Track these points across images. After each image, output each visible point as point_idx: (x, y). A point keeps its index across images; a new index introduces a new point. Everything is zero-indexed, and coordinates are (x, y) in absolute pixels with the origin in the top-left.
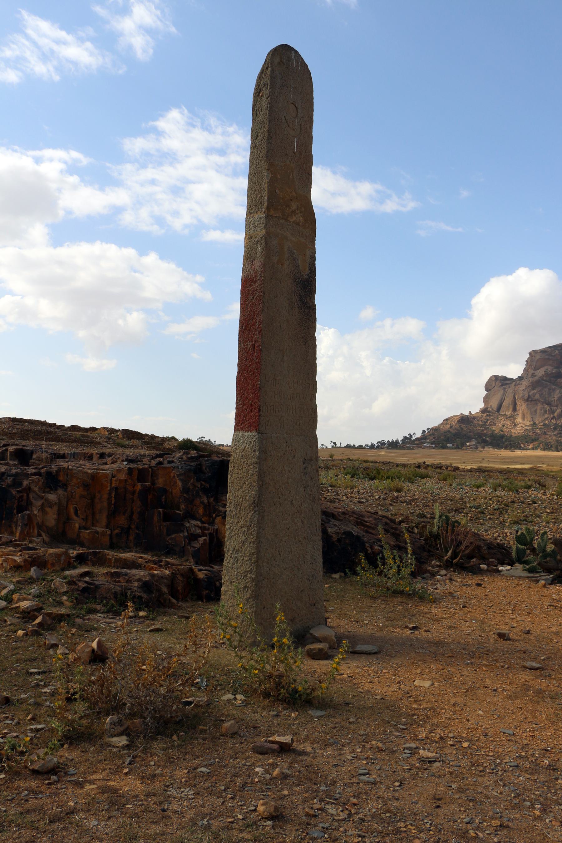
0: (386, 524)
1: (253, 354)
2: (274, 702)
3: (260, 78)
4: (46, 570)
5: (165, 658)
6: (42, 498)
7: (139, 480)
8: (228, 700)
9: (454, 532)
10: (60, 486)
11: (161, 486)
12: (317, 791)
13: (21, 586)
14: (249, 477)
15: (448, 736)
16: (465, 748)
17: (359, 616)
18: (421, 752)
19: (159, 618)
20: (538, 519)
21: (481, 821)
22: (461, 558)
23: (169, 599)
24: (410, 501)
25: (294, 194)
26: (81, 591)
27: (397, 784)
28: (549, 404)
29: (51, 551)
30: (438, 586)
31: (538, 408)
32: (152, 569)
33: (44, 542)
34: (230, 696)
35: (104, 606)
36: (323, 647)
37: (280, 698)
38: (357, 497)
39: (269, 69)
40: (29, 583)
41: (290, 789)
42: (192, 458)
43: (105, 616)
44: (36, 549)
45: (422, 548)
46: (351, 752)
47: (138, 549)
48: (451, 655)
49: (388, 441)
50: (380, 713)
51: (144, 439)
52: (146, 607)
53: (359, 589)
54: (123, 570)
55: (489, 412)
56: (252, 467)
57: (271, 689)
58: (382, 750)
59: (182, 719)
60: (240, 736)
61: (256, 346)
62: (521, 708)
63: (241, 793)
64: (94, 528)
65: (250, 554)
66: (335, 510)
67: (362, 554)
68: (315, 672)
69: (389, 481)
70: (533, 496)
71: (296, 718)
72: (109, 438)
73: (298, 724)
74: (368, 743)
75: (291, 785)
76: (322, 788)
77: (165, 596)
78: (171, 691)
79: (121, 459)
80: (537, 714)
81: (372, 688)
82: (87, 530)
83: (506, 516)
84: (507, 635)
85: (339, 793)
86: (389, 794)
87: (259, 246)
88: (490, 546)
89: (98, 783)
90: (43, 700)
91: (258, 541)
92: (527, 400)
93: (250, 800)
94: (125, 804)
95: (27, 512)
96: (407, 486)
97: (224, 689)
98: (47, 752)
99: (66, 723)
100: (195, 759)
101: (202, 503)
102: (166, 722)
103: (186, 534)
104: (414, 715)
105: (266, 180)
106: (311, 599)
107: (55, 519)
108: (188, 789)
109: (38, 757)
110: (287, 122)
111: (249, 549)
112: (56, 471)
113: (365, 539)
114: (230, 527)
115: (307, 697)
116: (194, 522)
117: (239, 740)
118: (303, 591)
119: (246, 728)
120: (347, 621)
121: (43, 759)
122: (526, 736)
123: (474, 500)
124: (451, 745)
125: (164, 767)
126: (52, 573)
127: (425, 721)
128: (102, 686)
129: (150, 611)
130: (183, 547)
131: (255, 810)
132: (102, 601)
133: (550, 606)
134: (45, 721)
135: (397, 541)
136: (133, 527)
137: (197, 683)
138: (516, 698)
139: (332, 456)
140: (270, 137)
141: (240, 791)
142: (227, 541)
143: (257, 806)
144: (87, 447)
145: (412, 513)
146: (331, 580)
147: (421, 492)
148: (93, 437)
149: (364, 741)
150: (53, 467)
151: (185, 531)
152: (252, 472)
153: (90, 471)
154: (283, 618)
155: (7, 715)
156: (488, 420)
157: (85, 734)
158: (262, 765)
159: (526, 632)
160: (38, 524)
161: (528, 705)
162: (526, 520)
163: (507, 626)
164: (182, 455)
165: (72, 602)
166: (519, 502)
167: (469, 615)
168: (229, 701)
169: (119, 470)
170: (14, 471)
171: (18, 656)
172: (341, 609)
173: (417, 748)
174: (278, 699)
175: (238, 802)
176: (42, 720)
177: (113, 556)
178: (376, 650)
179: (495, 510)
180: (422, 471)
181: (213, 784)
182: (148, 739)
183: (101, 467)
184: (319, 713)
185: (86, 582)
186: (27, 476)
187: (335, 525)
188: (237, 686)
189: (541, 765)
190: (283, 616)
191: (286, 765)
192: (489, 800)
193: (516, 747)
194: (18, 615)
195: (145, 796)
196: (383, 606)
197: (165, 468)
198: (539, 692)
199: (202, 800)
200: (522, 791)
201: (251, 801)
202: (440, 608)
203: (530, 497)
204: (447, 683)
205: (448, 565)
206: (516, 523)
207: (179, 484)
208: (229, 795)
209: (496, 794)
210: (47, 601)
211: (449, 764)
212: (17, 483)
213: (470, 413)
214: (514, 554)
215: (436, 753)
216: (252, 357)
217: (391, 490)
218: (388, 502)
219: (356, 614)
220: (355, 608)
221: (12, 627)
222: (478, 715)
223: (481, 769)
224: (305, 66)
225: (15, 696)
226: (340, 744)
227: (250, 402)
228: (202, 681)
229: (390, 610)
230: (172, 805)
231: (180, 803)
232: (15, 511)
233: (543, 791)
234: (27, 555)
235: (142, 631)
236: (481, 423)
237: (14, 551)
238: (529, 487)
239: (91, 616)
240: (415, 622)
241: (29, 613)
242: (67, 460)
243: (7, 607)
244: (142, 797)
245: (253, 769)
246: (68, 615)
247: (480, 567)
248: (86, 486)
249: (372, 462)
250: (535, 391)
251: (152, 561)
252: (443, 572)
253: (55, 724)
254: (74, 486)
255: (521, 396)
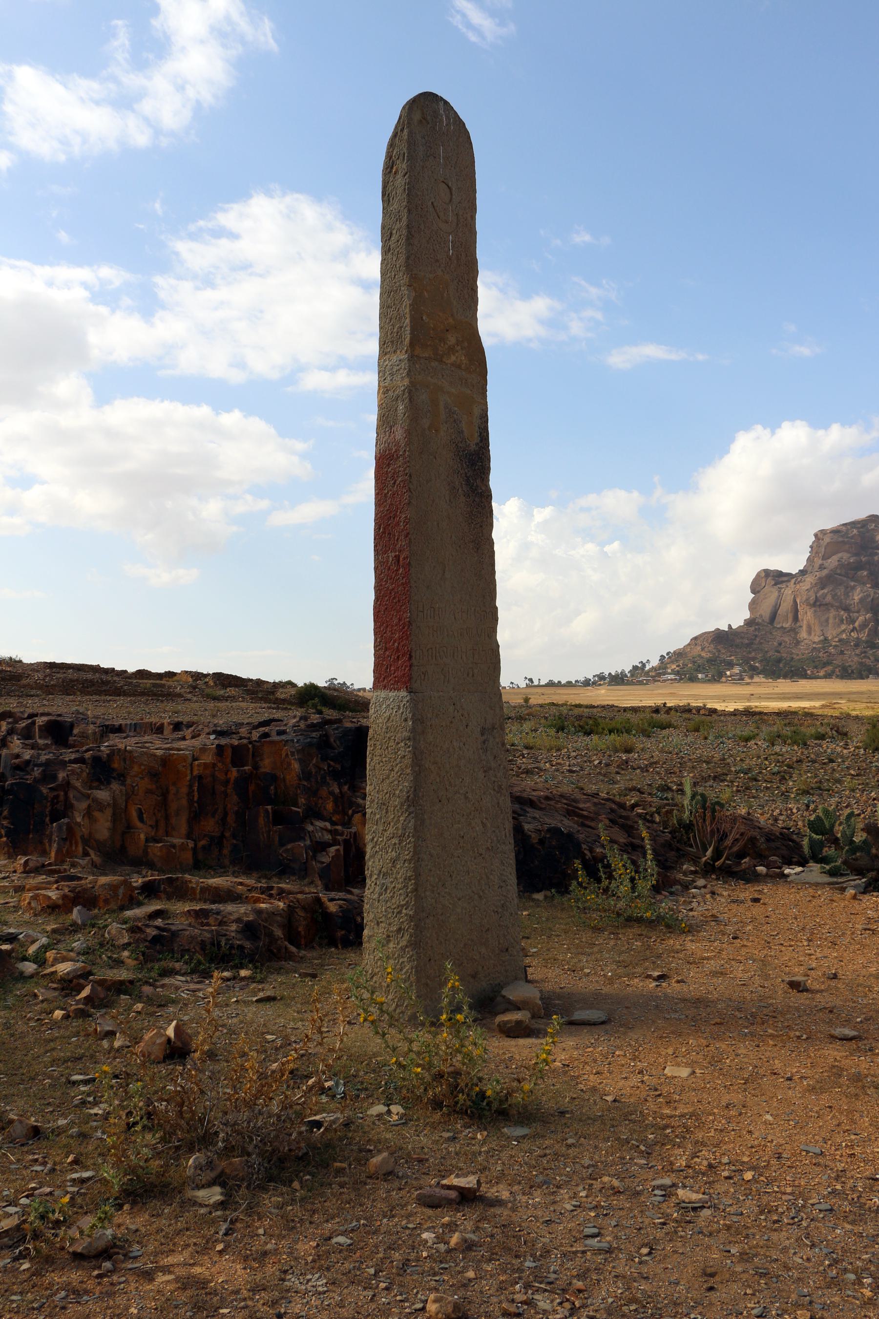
0: (612, 810)
1: (397, 570)
2: (449, 1115)
3: (392, 145)
4: (96, 911)
5: (281, 1047)
6: (88, 797)
7: (234, 764)
8: (377, 1116)
9: (714, 819)
10: (114, 778)
11: (267, 770)
12: (520, 1270)
13: (59, 937)
14: (398, 760)
15: (720, 1162)
16: (748, 1181)
17: (575, 960)
18: (680, 1192)
19: (271, 978)
20: (839, 786)
21: (779, 1312)
22: (727, 859)
23: (286, 948)
24: (646, 766)
25: (451, 320)
26: (150, 942)
27: (645, 1251)
28: (847, 609)
29: (103, 880)
30: (695, 905)
31: (831, 615)
32: (258, 900)
33: (94, 864)
34: (381, 1108)
35: (186, 963)
36: (523, 1019)
37: (458, 1109)
38: (564, 769)
39: (406, 131)
40: (71, 932)
41: (477, 1269)
42: (313, 725)
43: (189, 979)
44: (80, 879)
45: (668, 845)
46: (570, 1198)
47: (236, 869)
48: (718, 1020)
49: (610, 674)
50: (613, 1126)
51: (246, 686)
52: (250, 962)
53: (574, 916)
54: (214, 907)
55: (758, 624)
56: (403, 744)
57: (444, 1095)
58: (619, 1192)
59: (306, 1154)
60: (398, 1177)
61: (401, 559)
62: (830, 1107)
63: (401, 1278)
64: (168, 839)
65: (405, 879)
66: (534, 793)
67: (577, 861)
68: (511, 1058)
69: (613, 736)
70: (829, 750)
71: (484, 1142)
72: (195, 688)
73: (488, 1152)
74: (596, 1179)
75: (479, 1261)
76: (527, 1264)
77: (279, 942)
78: (286, 1106)
79: (207, 730)
80: (857, 1116)
81: (600, 1083)
82: (158, 843)
83: (791, 783)
84: (802, 984)
85: (555, 1272)
86: (632, 1270)
87: (400, 403)
88: (770, 837)
89: (176, 1270)
90: (91, 1127)
91: (417, 858)
92: (814, 605)
93: (415, 1291)
94: (219, 1308)
95: (66, 820)
96: (639, 742)
97: (372, 1096)
98: (94, 1225)
99: (126, 1170)
100: (327, 1221)
101: (332, 793)
102: (282, 1160)
103: (308, 842)
104: (666, 1127)
105: (407, 302)
106: (501, 941)
107: (109, 829)
108: (317, 1276)
109: (81, 1232)
110: (436, 210)
111: (403, 870)
112: (107, 755)
113: (581, 837)
114: (373, 838)
115: (500, 1105)
116: (320, 824)
117: (396, 1184)
118: (488, 930)
119: (407, 1162)
120: (557, 971)
121: (89, 1236)
122: (841, 1156)
123: (741, 760)
124: (726, 1178)
125: (281, 1237)
126: (105, 914)
127: (684, 1138)
128: (181, 1105)
129: (256, 968)
130: (305, 863)
131: (423, 1309)
132: (183, 956)
133: (865, 929)
134: (94, 1164)
135: (629, 836)
136: (227, 834)
137: (330, 1088)
138: (823, 1091)
139: (527, 700)
140: (410, 237)
141: (399, 1275)
142: (369, 860)
143: (427, 1301)
144: (162, 701)
145: (650, 785)
146: (531, 904)
147: (662, 751)
148: (170, 687)
149: (591, 1177)
150: (102, 748)
151: (307, 838)
152: (403, 753)
153: (159, 753)
154: (457, 983)
155: (36, 1157)
156: (756, 636)
157: (156, 1186)
158: (433, 1227)
159: (832, 976)
160: (82, 837)
161: (841, 1102)
162: (819, 788)
163: (802, 968)
164: (298, 722)
165: (136, 959)
166: (809, 761)
167: (743, 951)
168: (380, 1116)
169: (203, 749)
170: (43, 758)
171: (55, 1054)
172: (548, 950)
173: (674, 1185)
174: (454, 1111)
175: (396, 1296)
176: (90, 1162)
177: (197, 883)
178: (604, 1018)
179: (774, 774)
180: (662, 717)
181: (357, 1265)
182: (254, 1189)
183: (176, 745)
184: (520, 1131)
185: (157, 927)
186: (64, 764)
187: (534, 818)
188: (391, 1090)
189: (867, 1206)
190: (457, 981)
191: (469, 1225)
192: (791, 1274)
193: (826, 1176)
194: (55, 986)
195: (249, 1290)
196: (612, 943)
197: (273, 743)
198: (857, 1078)
199: (340, 1295)
200: (840, 1253)
201: (417, 1293)
202: (699, 941)
203: (825, 752)
204: (714, 1070)
205: (708, 870)
206: (806, 792)
207: (296, 766)
208: (381, 1284)
209: (800, 1261)
210: (99, 961)
211: (724, 1211)
212: (48, 776)
213: (730, 626)
214: (806, 850)
215: (704, 1194)
216: (396, 575)
217: (616, 751)
218: (613, 769)
219: (572, 958)
220: (569, 949)
221: (45, 1005)
222: (765, 1122)
223: (775, 1218)
224: (460, 124)
225: (49, 1122)
226: (554, 1185)
227: (396, 644)
228: (337, 1084)
229: (623, 949)
230: (293, 1304)
231: (305, 1301)
232: (48, 819)
233: (873, 1253)
234: (66, 887)
235: (244, 1002)
236: (747, 641)
237: (49, 883)
238: (822, 737)
239: (166, 981)
240: (662, 967)
241: (71, 981)
242: (125, 735)
243: (38, 973)
244: (245, 1293)
245: (419, 1235)
246: (131, 982)
247: (756, 871)
248: (154, 775)
249: (587, 707)
250: (826, 591)
251: (257, 888)
252: (701, 882)
253: (108, 1172)
254: (135, 776)
255: (804, 599)
